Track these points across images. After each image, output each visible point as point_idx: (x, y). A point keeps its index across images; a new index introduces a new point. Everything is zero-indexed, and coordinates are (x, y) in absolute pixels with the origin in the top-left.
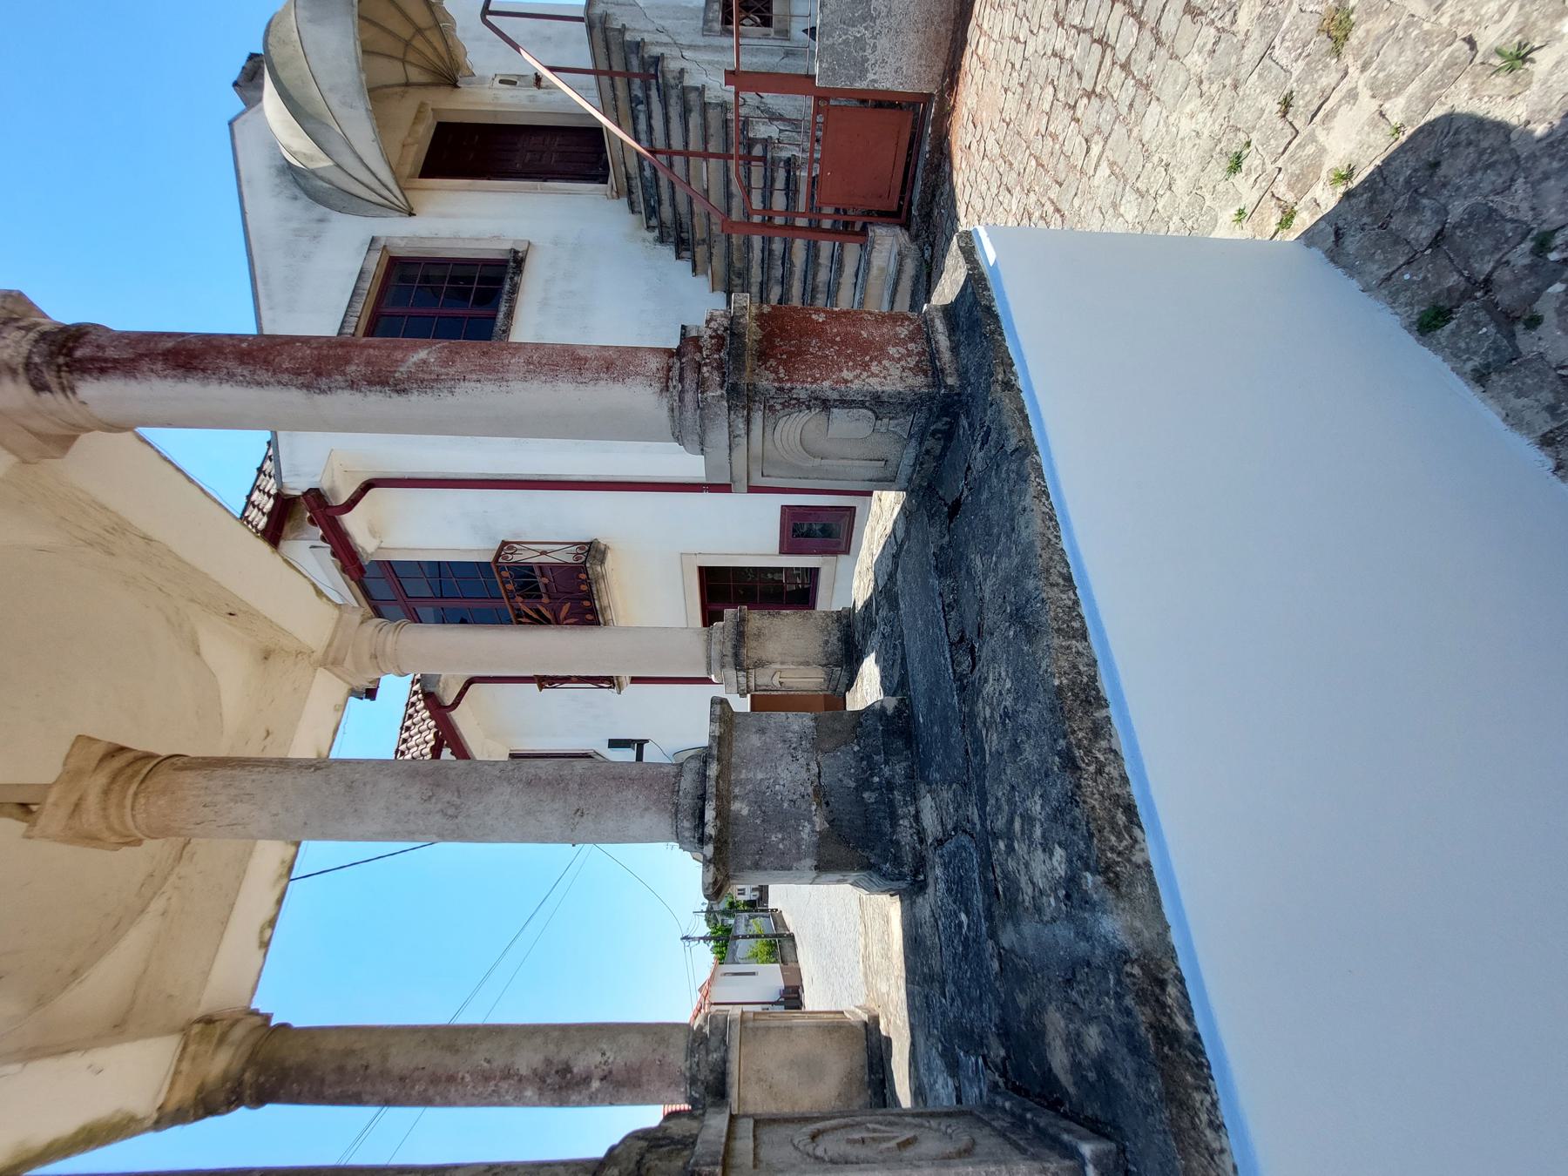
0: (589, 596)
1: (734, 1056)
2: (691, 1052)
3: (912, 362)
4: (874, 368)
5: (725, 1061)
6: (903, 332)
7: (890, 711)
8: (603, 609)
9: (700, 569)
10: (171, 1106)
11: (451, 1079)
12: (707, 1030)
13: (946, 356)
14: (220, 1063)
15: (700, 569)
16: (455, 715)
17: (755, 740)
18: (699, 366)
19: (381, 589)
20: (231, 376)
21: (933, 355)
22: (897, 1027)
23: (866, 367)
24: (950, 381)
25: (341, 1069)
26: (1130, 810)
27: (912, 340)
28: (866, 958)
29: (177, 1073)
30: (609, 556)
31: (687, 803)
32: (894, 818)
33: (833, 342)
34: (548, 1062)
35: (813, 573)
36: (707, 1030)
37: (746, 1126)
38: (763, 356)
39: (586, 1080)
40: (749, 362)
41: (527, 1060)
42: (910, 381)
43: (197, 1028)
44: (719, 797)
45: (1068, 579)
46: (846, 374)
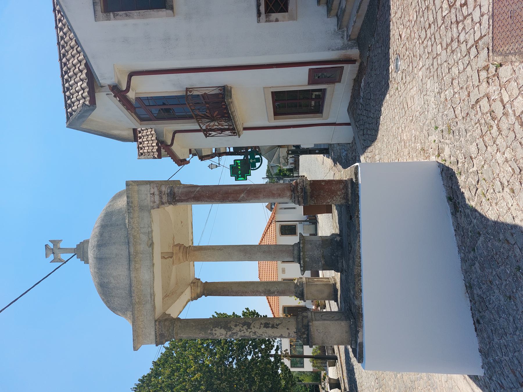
0: (226, 108)
1: (305, 289)
2: (295, 288)
3: (342, 196)
4: (334, 199)
5: (303, 290)
6: (341, 187)
7: (338, 240)
8: (232, 113)
9: (272, 92)
10: (193, 297)
11: (246, 292)
12: (298, 284)
13: (350, 195)
14: (199, 290)
15: (272, 92)
16: (173, 148)
17: (310, 246)
18: (298, 197)
19: (142, 112)
20: (207, 201)
21: (347, 195)
22: (338, 286)
23: (333, 198)
24: (350, 203)
25: (223, 291)
26: (361, 290)
27: (343, 189)
28: (378, 8)
29: (192, 292)
30: (233, 92)
31: (296, 256)
32: (338, 262)
33: (326, 191)
34: (265, 289)
35: (323, 91)
36: (298, 284)
37: (313, 313)
38: (311, 197)
39: (274, 292)
40: (309, 199)
41: (261, 289)
42: (341, 202)
43: (192, 284)
44: (303, 259)
45: (360, 257)
46: (329, 201)
